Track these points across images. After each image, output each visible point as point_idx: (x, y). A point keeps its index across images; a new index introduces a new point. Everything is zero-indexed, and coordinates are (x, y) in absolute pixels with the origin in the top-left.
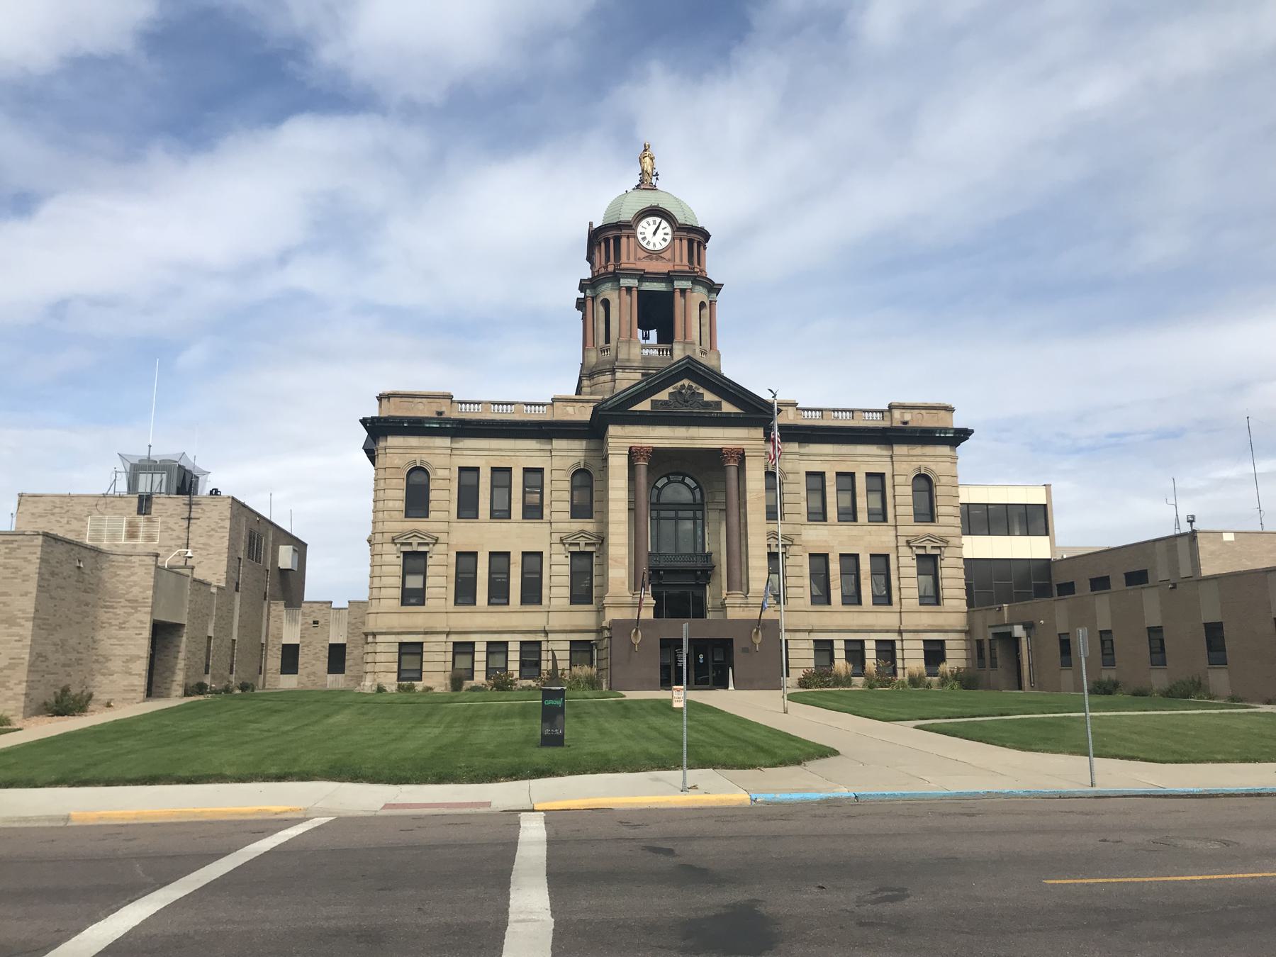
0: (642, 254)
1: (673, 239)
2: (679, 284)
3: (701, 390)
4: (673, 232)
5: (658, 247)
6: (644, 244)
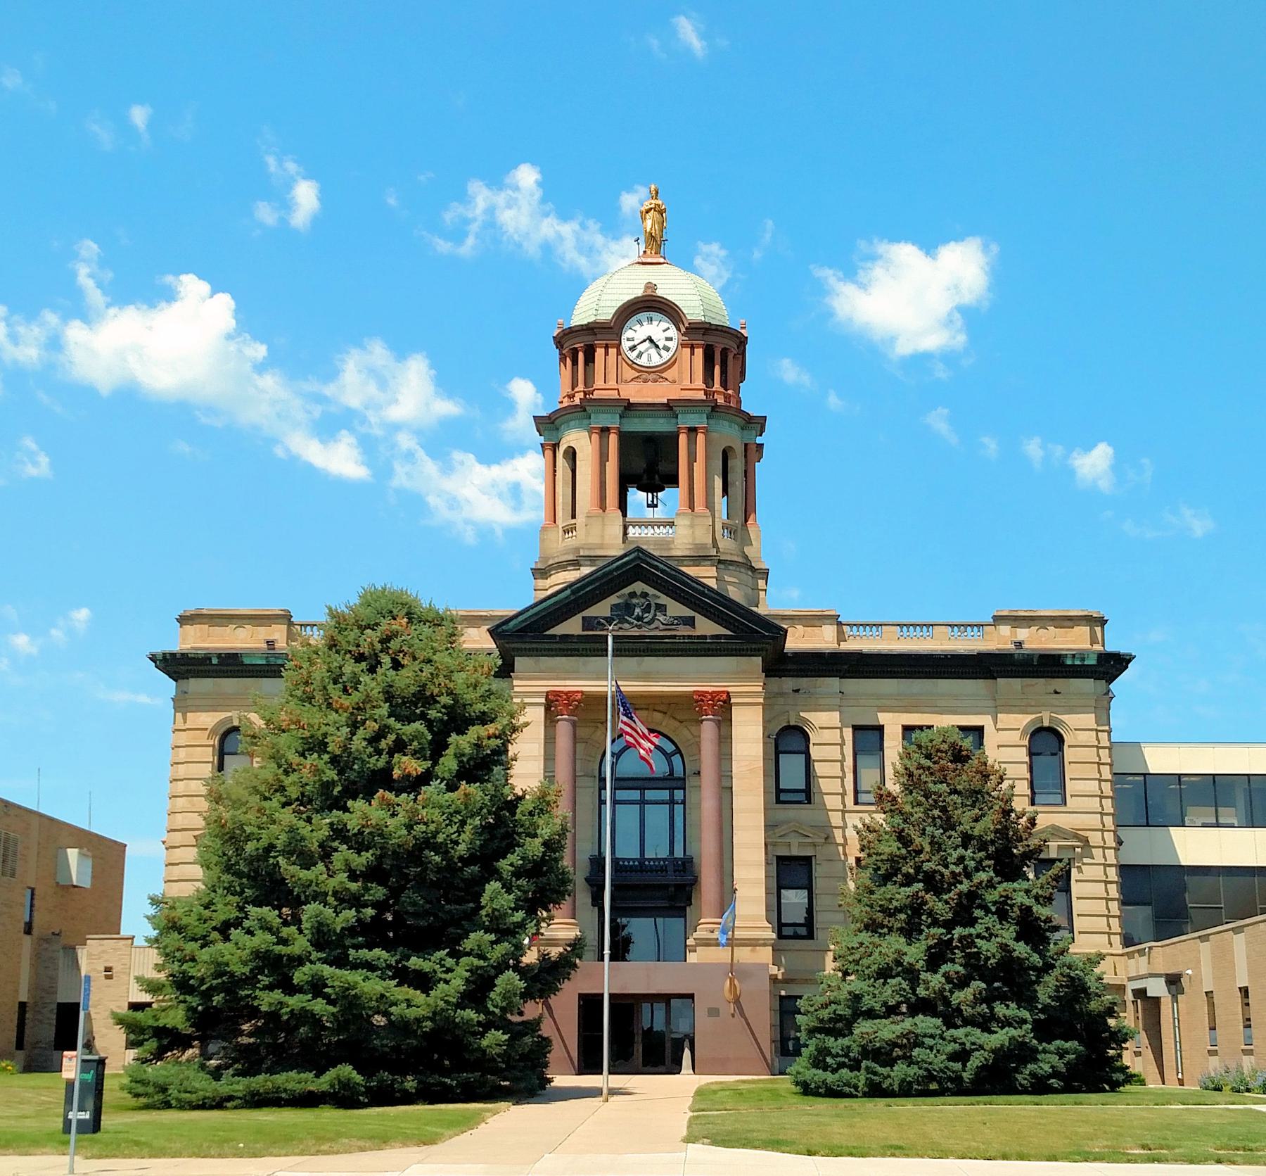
0: (629, 373)
2: (686, 420)
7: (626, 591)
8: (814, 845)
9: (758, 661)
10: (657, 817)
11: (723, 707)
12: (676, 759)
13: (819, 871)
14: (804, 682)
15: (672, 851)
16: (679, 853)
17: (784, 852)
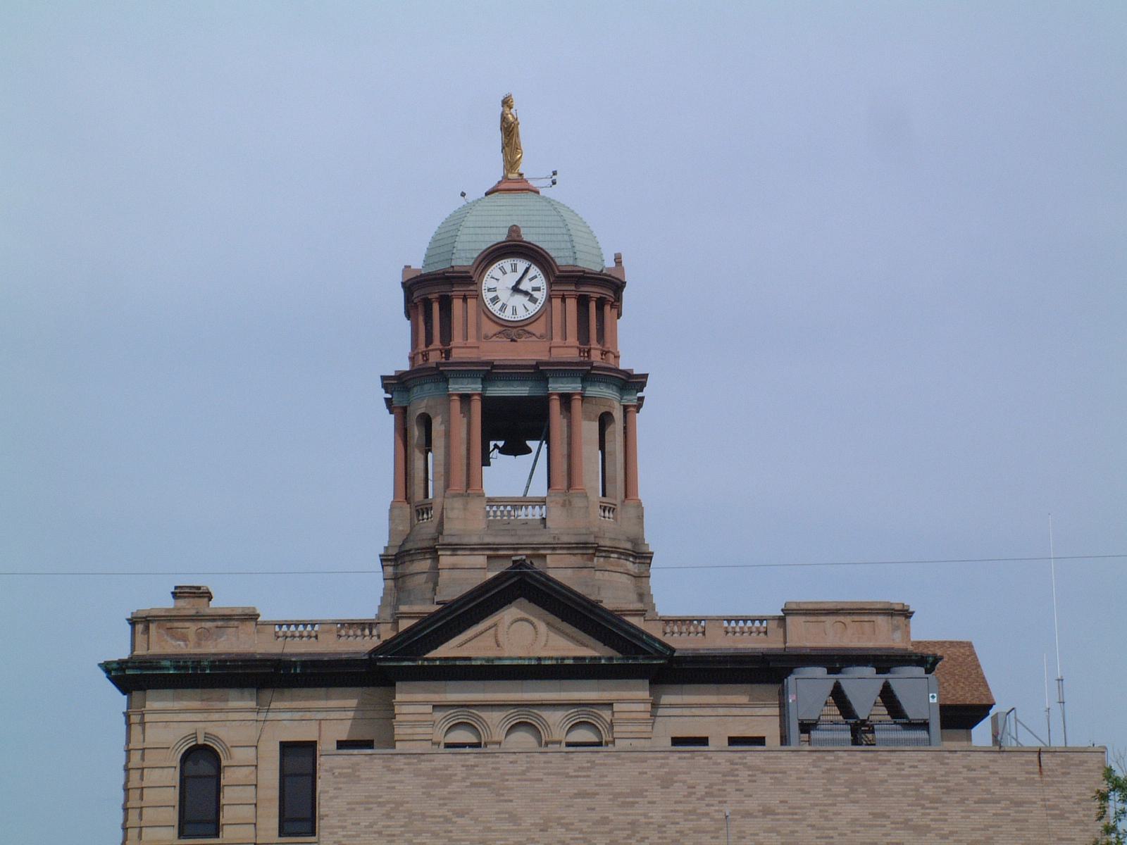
1: (550, 298)
2: (558, 387)
4: (550, 284)
5: (522, 315)
6: (495, 309)
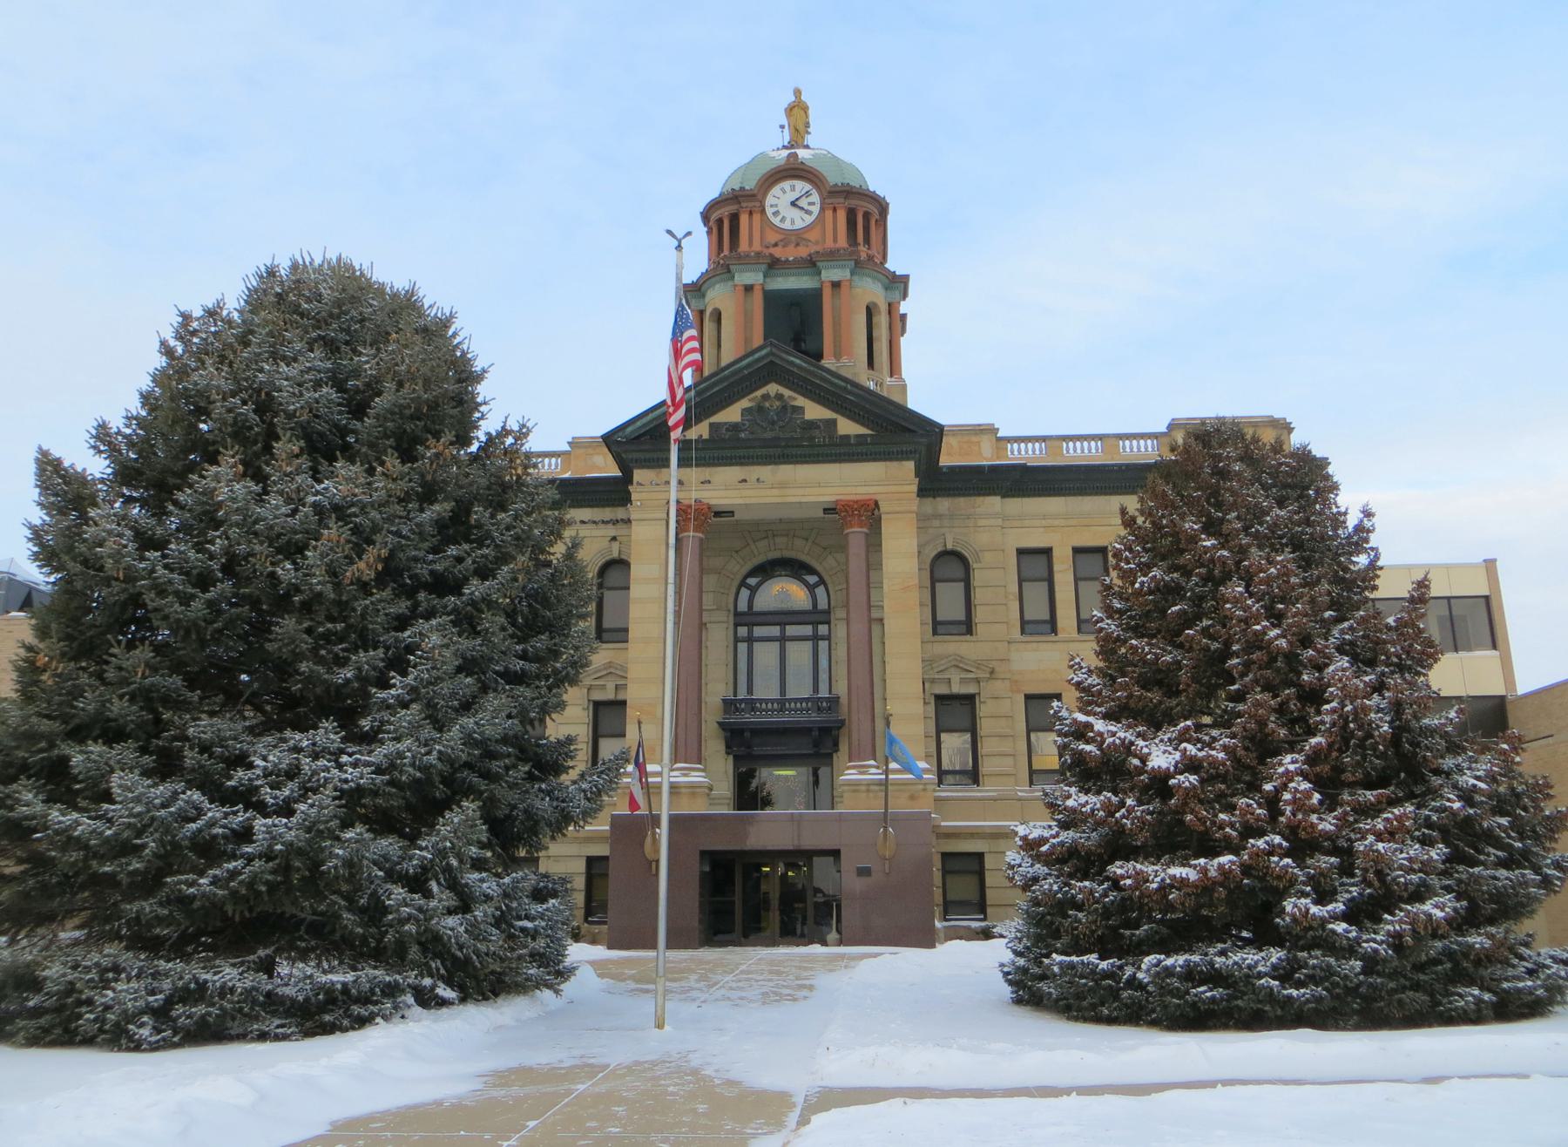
1: (822, 209)
2: (831, 274)
3: (801, 401)
6: (776, 221)
7: (759, 393)
8: (978, 681)
9: (910, 466)
10: (799, 654)
11: (868, 514)
12: (820, 591)
13: (983, 710)
14: (962, 502)
15: (816, 689)
16: (824, 693)
17: (942, 690)
